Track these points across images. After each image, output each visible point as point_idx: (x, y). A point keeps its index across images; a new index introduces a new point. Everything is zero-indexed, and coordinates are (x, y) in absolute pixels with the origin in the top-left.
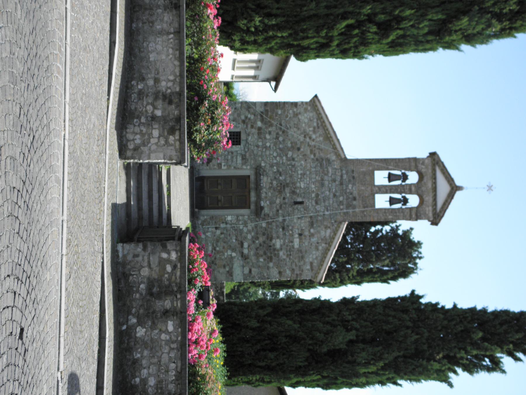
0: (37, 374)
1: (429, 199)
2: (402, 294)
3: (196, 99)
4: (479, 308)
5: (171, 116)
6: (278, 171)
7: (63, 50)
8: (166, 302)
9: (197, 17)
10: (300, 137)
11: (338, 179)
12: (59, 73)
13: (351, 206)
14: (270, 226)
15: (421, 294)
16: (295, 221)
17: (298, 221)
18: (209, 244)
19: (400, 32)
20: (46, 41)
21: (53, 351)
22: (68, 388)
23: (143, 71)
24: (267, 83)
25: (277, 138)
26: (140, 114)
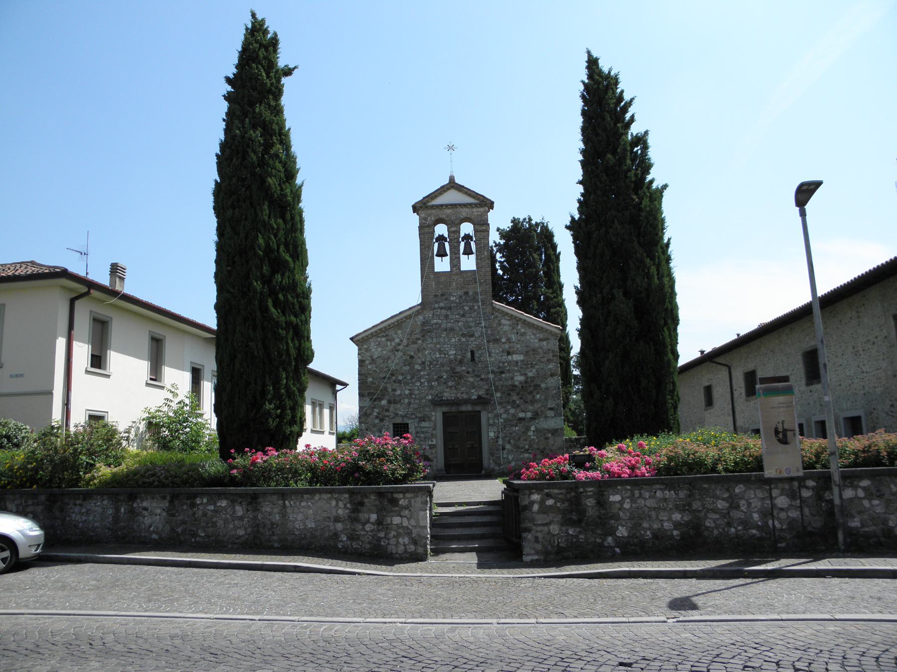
0: (669, 646)
1: (464, 212)
2: (571, 239)
3: (357, 475)
4: (581, 158)
5: (377, 503)
6: (437, 380)
7: (305, 624)
9: (266, 474)
12: (331, 630)
15: (570, 219)
16: (493, 359)
17: (493, 356)
19: (282, 248)
20: (296, 643)
21: (643, 630)
22: (685, 610)
23: (327, 535)
25: (400, 382)
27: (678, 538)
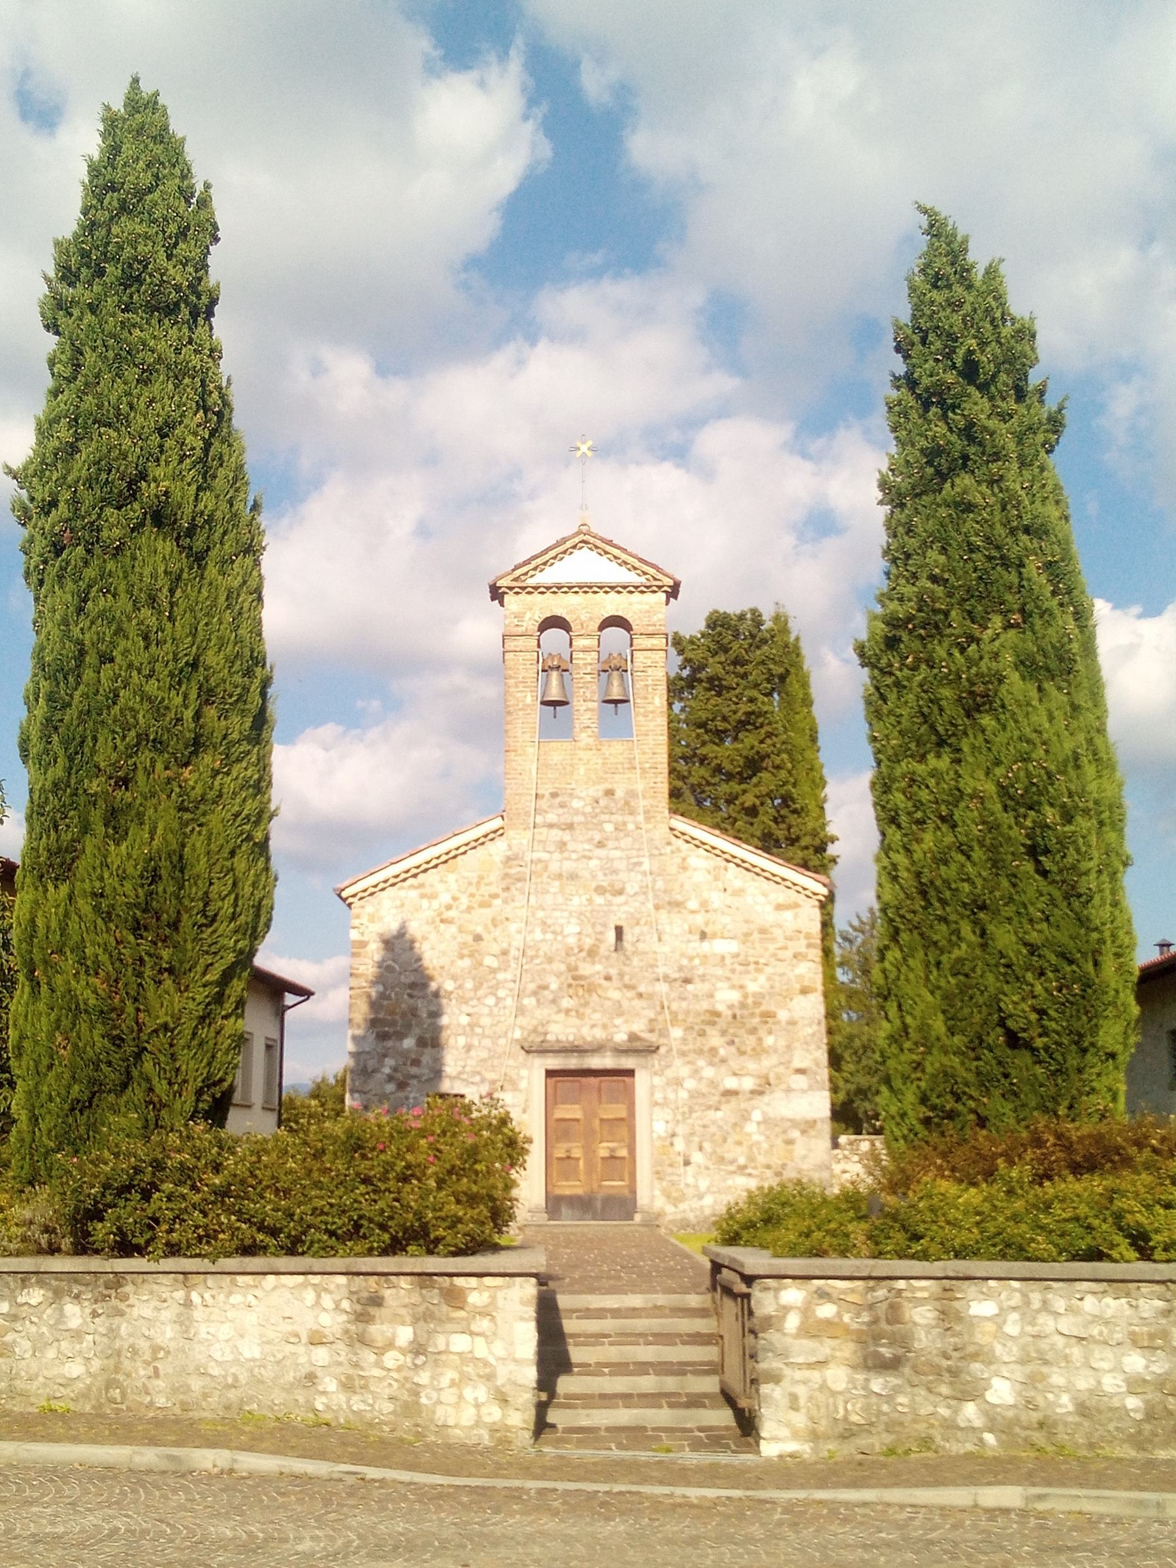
6: (534, 993)
8: (918, 1319)
10: (447, 936)
11: (556, 834)
13: (627, 803)
14: (680, 1017)
16: (666, 949)
18: (730, 1182)
23: (290, 1376)
24: (288, 1014)
26: (408, 1386)
27: (1139, 1416)
